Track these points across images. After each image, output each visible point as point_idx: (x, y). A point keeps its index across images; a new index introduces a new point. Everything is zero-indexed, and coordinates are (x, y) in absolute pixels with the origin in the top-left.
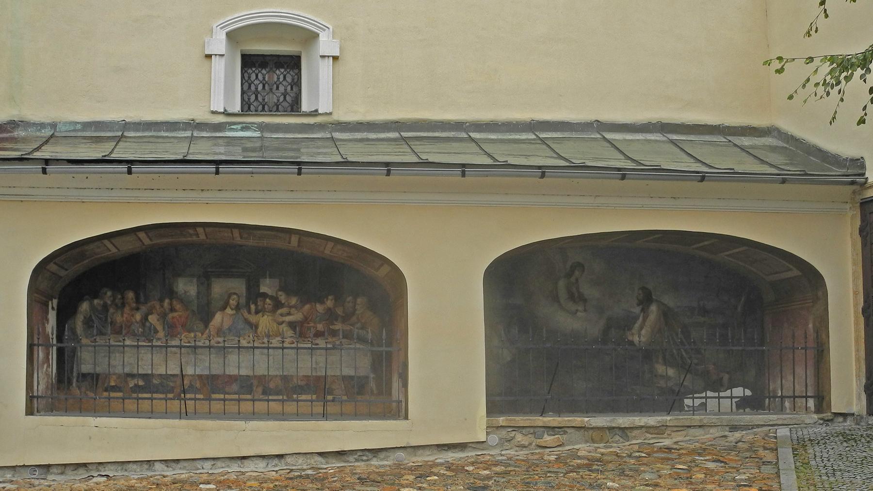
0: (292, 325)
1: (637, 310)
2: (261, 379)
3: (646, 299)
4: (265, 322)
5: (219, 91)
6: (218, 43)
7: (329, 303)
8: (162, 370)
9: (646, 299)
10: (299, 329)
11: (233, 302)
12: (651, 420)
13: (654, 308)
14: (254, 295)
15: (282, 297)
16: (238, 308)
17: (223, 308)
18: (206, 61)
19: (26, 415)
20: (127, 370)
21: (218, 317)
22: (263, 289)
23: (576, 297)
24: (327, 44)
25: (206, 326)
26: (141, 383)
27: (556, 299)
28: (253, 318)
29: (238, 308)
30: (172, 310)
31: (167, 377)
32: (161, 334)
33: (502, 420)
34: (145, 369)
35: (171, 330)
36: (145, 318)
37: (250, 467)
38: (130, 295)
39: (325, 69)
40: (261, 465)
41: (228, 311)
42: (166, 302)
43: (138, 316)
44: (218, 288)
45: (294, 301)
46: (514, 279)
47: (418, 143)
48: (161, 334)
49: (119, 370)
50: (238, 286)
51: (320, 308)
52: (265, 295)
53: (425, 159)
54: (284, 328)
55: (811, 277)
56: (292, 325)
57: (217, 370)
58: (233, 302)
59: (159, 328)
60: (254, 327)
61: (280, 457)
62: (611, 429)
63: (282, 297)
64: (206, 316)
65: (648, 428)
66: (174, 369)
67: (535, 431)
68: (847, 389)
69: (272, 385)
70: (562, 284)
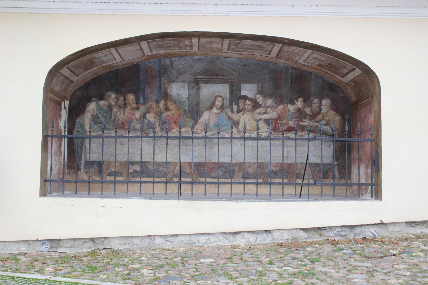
0: (267, 121)
7: (300, 104)
11: (218, 103)
14: (236, 97)
15: (260, 99)
16: (222, 108)
19: (43, 193)
21: (205, 116)
22: (244, 92)
28: (235, 116)
36: (144, 116)
40: (252, 238)
41: (214, 110)
43: (138, 115)
44: (208, 91)
45: (269, 102)
50: (223, 90)
51: (291, 108)
52: (245, 98)
54: (262, 124)
56: (267, 121)
58: (218, 103)
61: (268, 232)
63: (260, 99)
69: (251, 171)
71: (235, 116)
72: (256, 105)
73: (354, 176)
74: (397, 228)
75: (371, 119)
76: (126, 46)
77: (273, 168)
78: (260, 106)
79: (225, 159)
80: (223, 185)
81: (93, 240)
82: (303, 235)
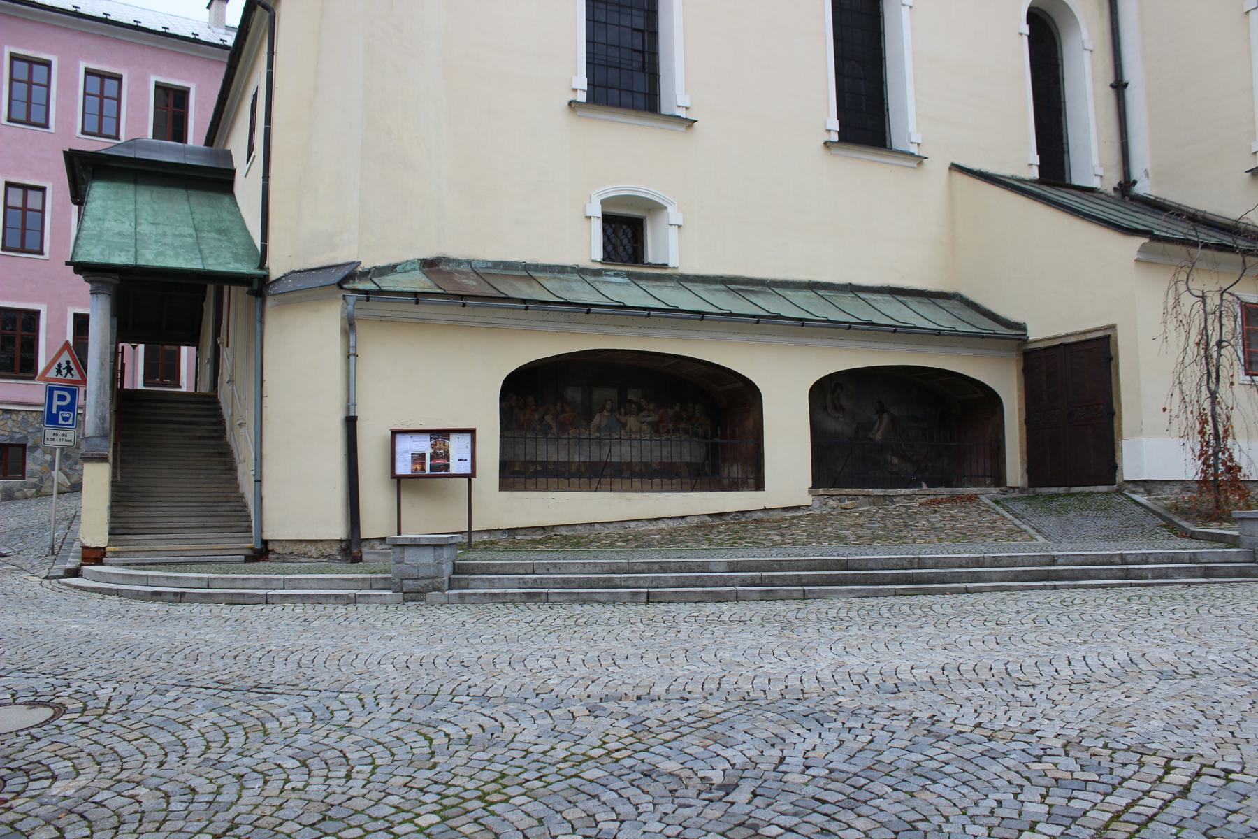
0: (649, 423)
1: (875, 417)
2: (629, 465)
3: (881, 410)
4: (632, 421)
5: (588, 246)
6: (597, 211)
7: (677, 408)
8: (555, 459)
9: (881, 410)
10: (656, 428)
11: (608, 407)
12: (907, 491)
13: (885, 416)
14: (623, 402)
15: (644, 403)
16: (612, 411)
17: (601, 411)
18: (586, 221)
19: (503, 487)
20: (528, 458)
21: (597, 418)
22: (630, 397)
23: (838, 408)
24: (674, 215)
25: (589, 426)
26: (539, 468)
27: (825, 408)
28: (623, 419)
29: (612, 411)
30: (563, 411)
31: (557, 463)
32: (555, 430)
33: (821, 491)
34: (541, 457)
35: (563, 428)
36: (542, 418)
37: (662, 525)
38: (531, 399)
39: (673, 233)
40: (670, 523)
41: (605, 413)
42: (559, 405)
43: (537, 417)
44: (598, 395)
45: (652, 406)
46: (824, 393)
47: (548, 275)
48: (555, 430)
49: (522, 458)
50: (612, 394)
51: (670, 412)
52: (631, 402)
53: (759, 306)
54: (645, 427)
55: (990, 400)
56: (649, 423)
57: (595, 458)
58: (608, 407)
59: (553, 425)
60: (624, 426)
61: (682, 517)
62: (884, 496)
63: (644, 403)
64: (589, 417)
65: (905, 496)
66: (563, 457)
67: (841, 498)
68: (1015, 471)
69: (637, 470)
70: (829, 397)
71: (623, 419)
72: (640, 409)
73: (725, 473)
74: (775, 513)
75: (750, 424)
76: (876, 345)
77: (655, 467)
78: (644, 410)
79: (615, 459)
80: (265, 529)
81: (543, 528)
82: (708, 519)
